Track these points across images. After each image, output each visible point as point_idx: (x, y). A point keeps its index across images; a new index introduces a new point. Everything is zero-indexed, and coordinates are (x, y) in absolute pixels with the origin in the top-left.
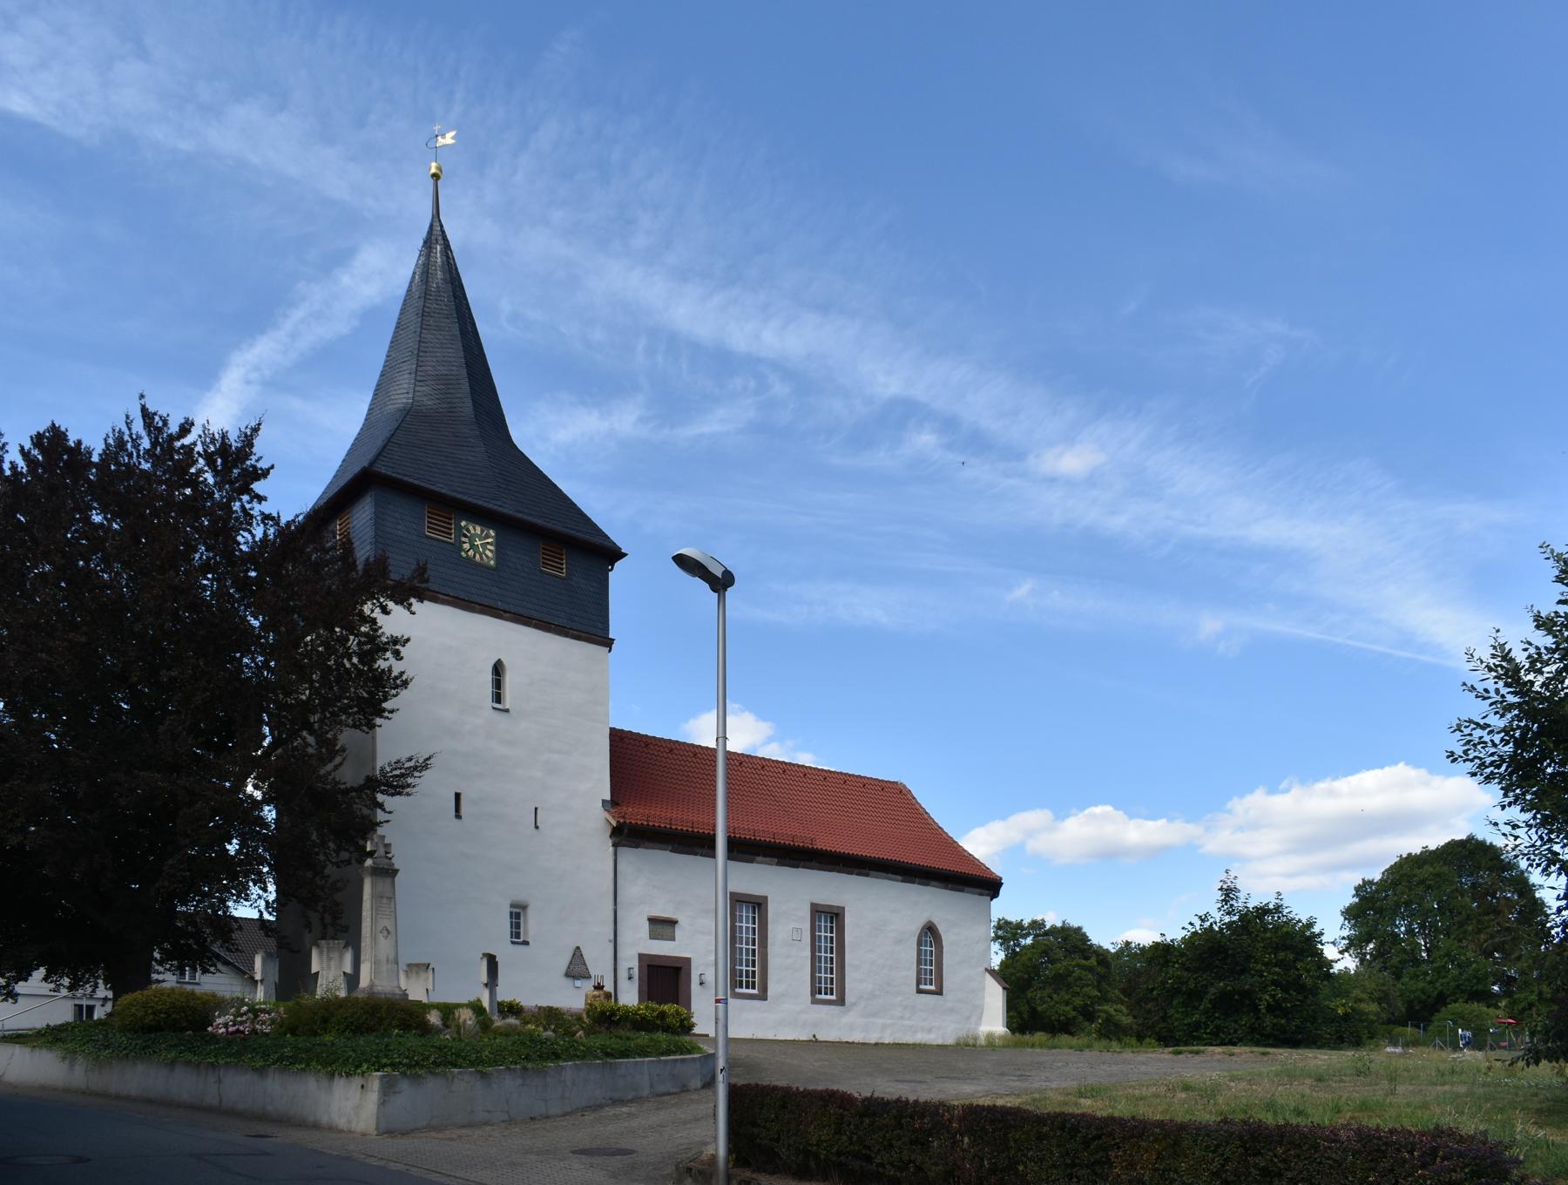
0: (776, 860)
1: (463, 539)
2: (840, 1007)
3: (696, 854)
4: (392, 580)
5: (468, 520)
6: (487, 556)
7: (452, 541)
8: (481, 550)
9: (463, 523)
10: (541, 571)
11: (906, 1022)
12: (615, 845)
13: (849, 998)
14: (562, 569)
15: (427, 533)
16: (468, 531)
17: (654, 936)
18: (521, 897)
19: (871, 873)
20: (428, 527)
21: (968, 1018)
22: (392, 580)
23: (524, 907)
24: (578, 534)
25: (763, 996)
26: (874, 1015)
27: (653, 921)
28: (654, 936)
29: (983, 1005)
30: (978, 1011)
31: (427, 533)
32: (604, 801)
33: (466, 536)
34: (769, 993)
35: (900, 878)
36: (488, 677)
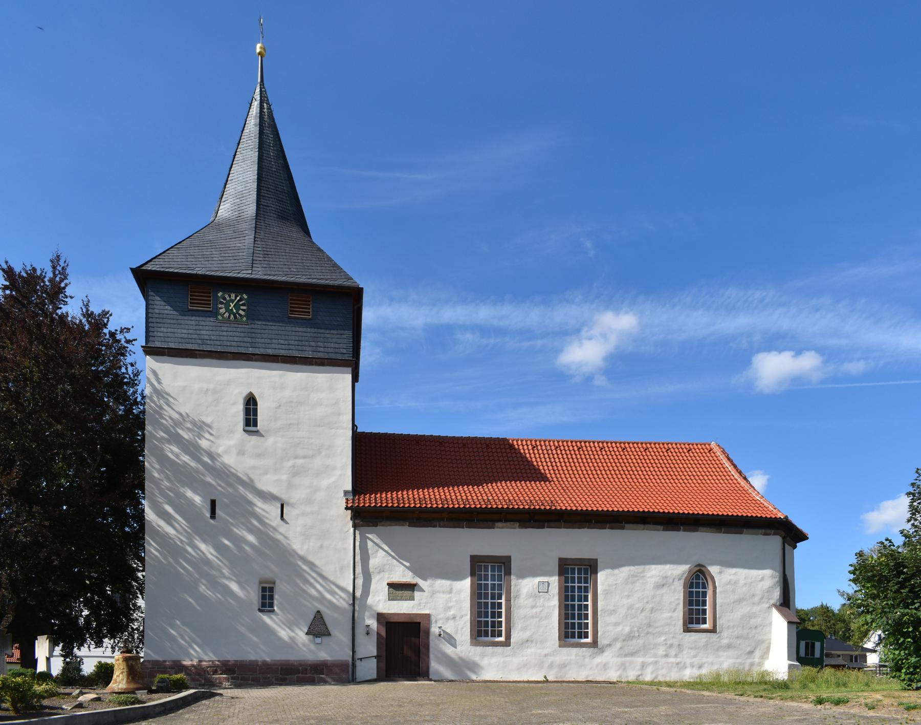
0: (518, 524)
1: (220, 306)
2: (564, 636)
3: (435, 526)
4: (160, 435)
5: (224, 291)
6: (240, 315)
7: (211, 309)
8: (235, 311)
9: (220, 294)
10: (290, 318)
11: (672, 660)
12: (355, 526)
13: (602, 641)
14: (309, 312)
15: (190, 308)
16: (224, 299)
17: (391, 598)
18: (213, 498)
19: (627, 526)
20: (191, 303)
21: (751, 653)
22: (160, 435)
23: (271, 590)
24: (327, 282)
25: (507, 643)
26: (632, 654)
27: (391, 585)
28: (391, 598)
29: (770, 639)
30: (763, 646)
31: (190, 308)
32: (346, 493)
33: (222, 303)
34: (512, 640)
35: (662, 527)
36: (240, 407)
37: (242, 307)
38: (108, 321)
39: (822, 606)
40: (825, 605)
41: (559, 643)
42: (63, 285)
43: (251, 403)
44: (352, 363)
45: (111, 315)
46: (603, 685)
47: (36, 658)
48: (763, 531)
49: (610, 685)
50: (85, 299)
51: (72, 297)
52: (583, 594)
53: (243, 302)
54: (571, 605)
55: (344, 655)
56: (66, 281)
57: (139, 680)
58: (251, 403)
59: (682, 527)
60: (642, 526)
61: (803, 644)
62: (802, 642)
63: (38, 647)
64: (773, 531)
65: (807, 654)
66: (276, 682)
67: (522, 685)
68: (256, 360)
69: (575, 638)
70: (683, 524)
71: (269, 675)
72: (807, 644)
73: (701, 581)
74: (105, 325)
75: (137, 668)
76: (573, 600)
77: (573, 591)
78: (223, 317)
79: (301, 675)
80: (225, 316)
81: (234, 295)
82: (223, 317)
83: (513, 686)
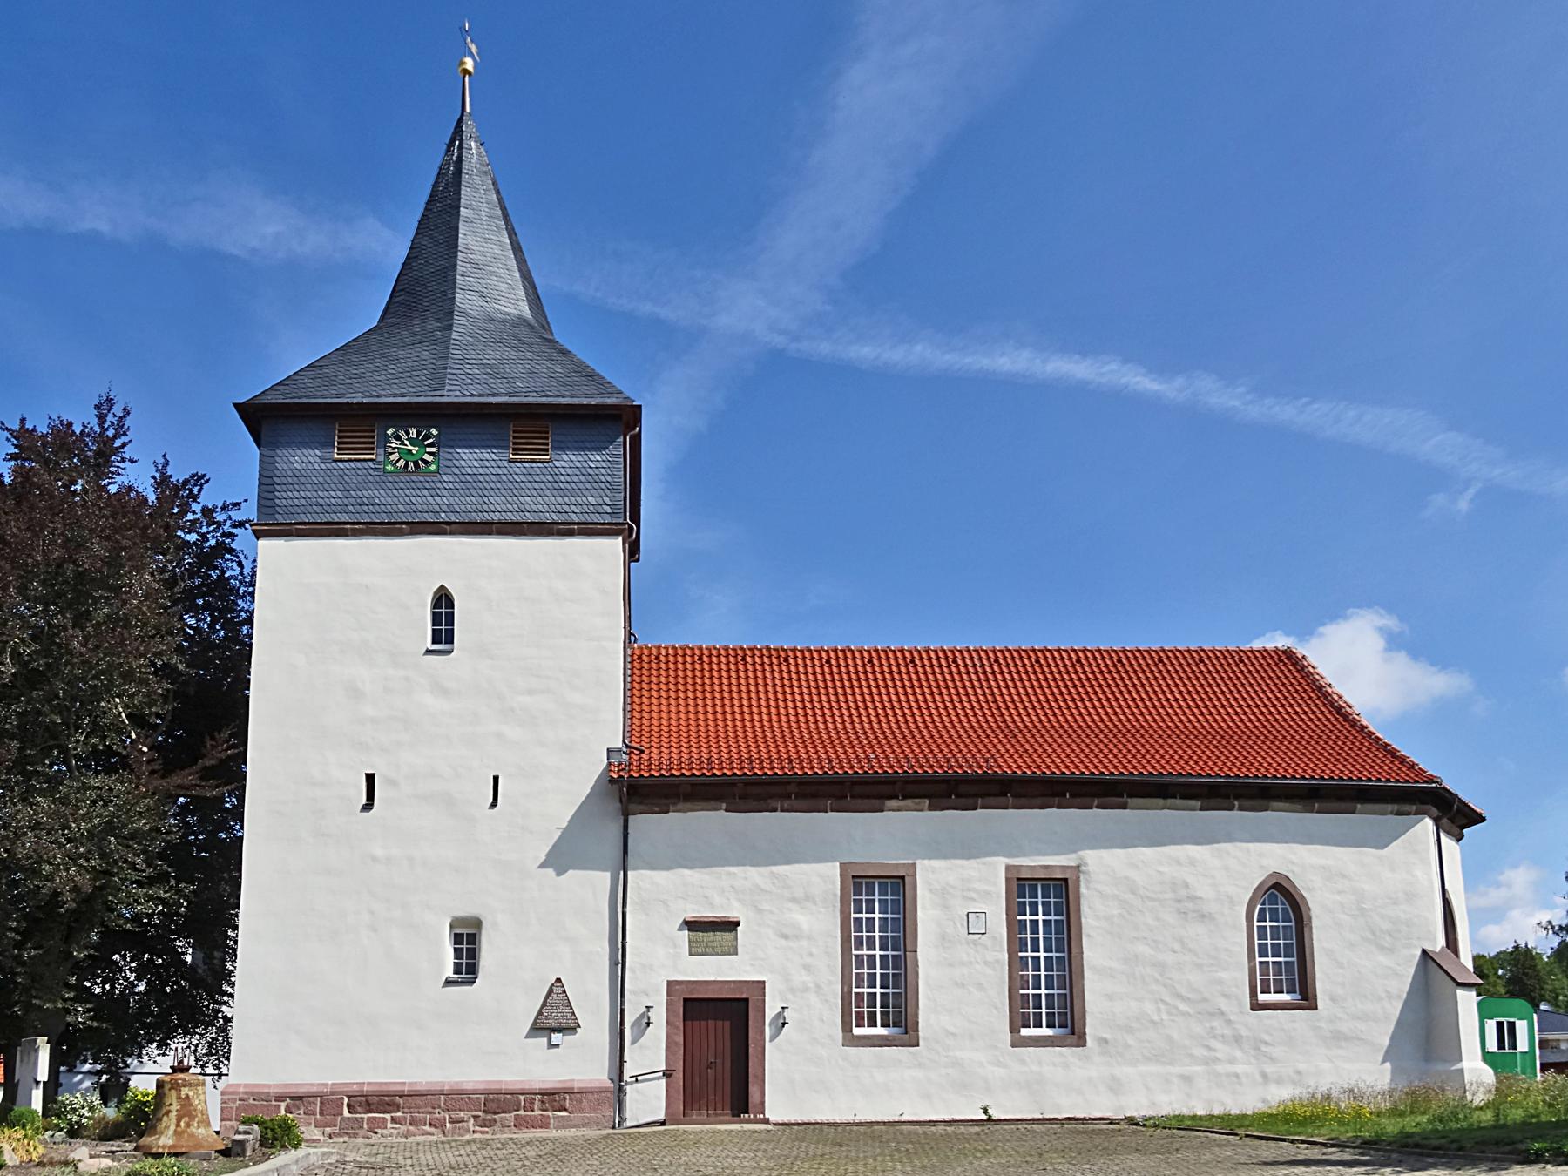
0: (927, 801)
7: (373, 457)
37: (428, 450)
38: (200, 491)
39: (1517, 947)
40: (1523, 945)
41: (1012, 1037)
42: (117, 444)
43: (443, 603)
44: (627, 527)
45: (207, 482)
46: (1098, 1126)
47: (16, 1079)
48: (1396, 807)
49: (1111, 1126)
50: (161, 460)
51: (132, 461)
52: (865, 934)
53: (431, 440)
54: (1033, 958)
55: (596, 1073)
56: (124, 439)
57: (199, 1127)
58: (443, 603)
59: (1236, 803)
60: (1161, 802)
61: (1491, 1026)
62: (1489, 1021)
63: (22, 1061)
64: (1414, 807)
65: (1501, 1045)
66: (477, 1128)
67: (941, 1128)
68: (452, 533)
69: (1041, 1027)
70: (1237, 797)
71: (462, 1114)
72: (1500, 1025)
73: (1280, 906)
74: (195, 498)
75: (197, 1102)
76: (1036, 949)
77: (871, 928)
78: (396, 467)
79: (521, 1112)
80: (398, 465)
81: (415, 431)
82: (396, 467)
83: (925, 1133)
